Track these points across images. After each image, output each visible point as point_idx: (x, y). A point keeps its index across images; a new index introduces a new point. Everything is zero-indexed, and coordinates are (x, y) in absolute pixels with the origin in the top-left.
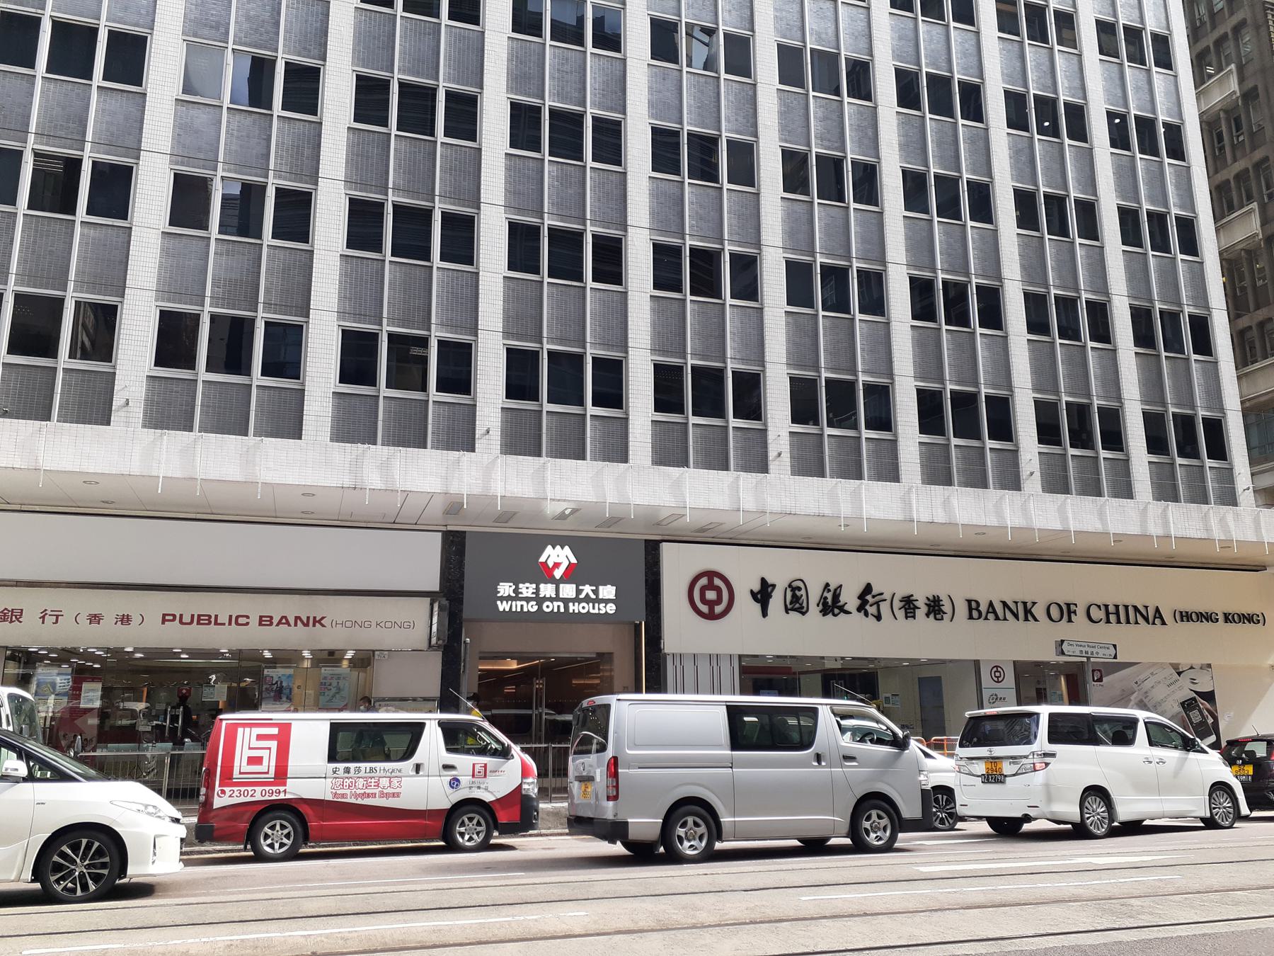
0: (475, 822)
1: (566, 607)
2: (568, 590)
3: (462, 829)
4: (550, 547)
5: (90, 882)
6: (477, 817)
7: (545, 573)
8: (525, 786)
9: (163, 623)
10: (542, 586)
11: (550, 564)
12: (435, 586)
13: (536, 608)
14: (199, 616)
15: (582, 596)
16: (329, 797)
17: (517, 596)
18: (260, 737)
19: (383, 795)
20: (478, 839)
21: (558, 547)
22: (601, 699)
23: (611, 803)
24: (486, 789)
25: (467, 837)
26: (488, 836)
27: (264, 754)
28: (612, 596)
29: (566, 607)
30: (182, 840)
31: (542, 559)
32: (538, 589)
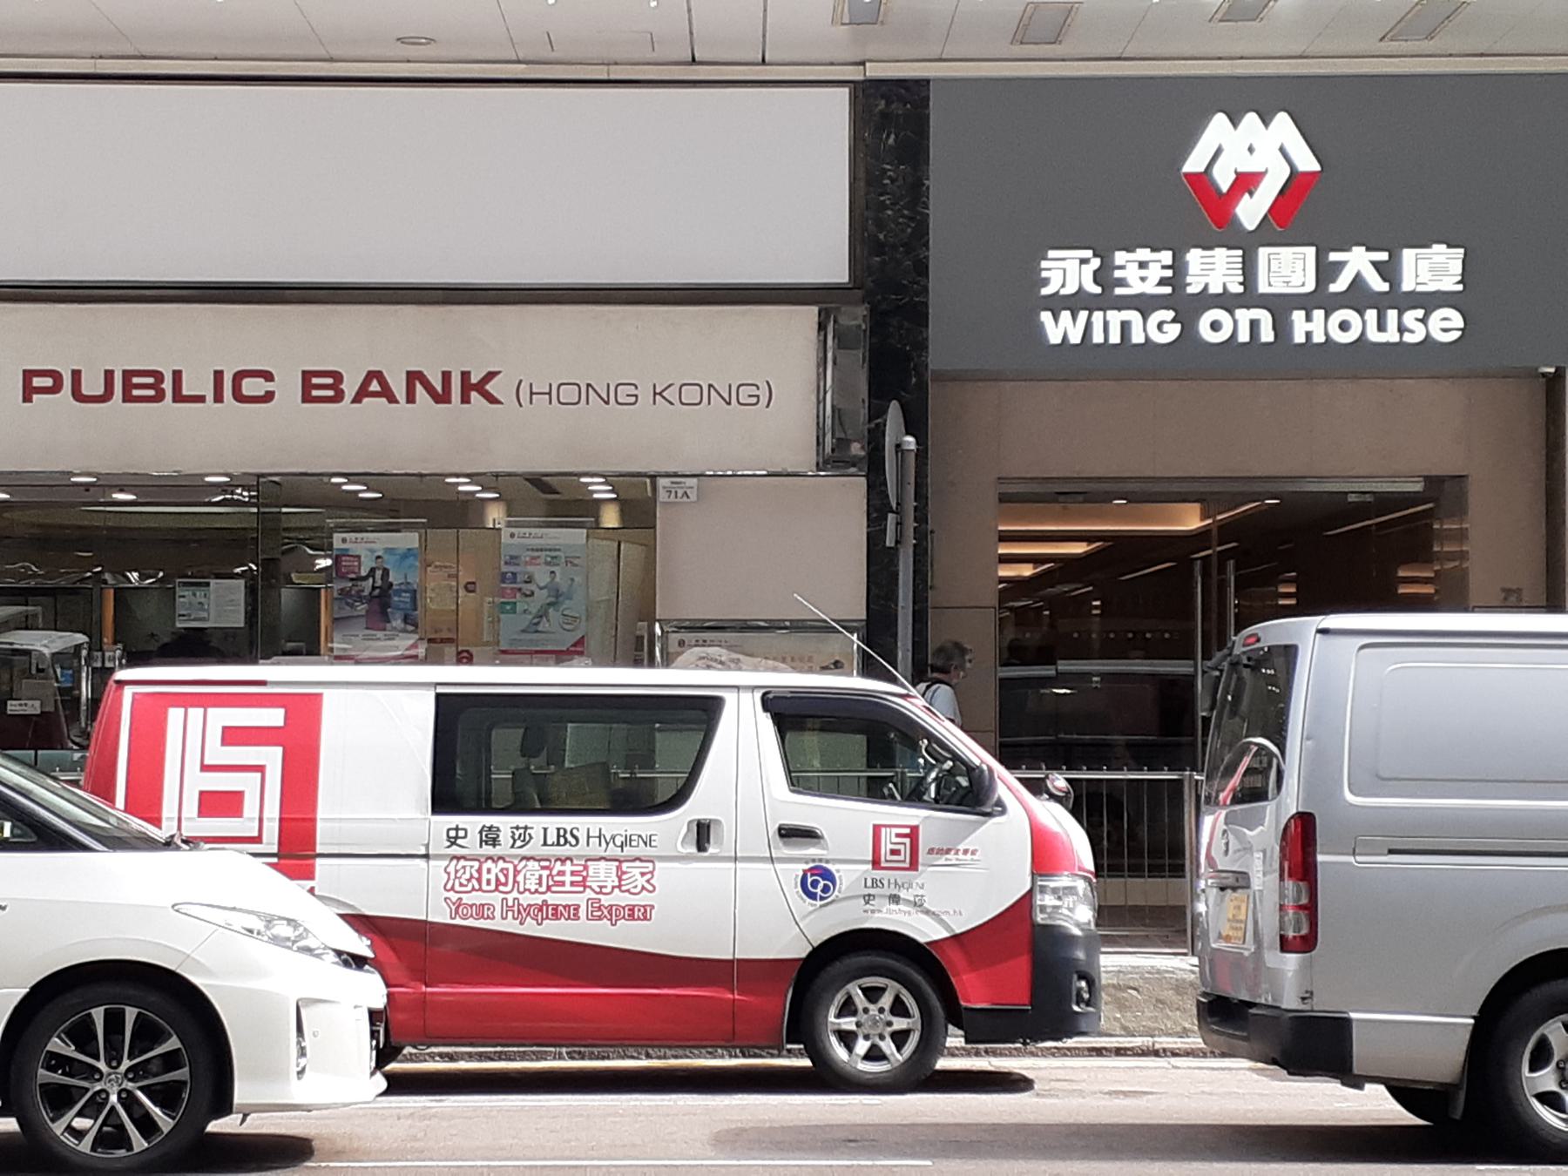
0: (886, 1001)
1: (1282, 327)
2: (1287, 269)
3: (848, 1023)
4: (1220, 120)
5: (156, 1111)
6: (893, 988)
7: (1208, 212)
8: (1039, 900)
9: (27, 398)
10: (1194, 257)
11: (1224, 179)
12: (836, 270)
13: (1173, 331)
14: (128, 375)
15: (1340, 285)
16: (441, 916)
17: (1107, 294)
18: (232, 736)
19: (600, 912)
20: (897, 1057)
21: (1251, 119)
22: (1274, 631)
23: (1292, 960)
24: (917, 904)
25: (862, 1046)
26: (930, 1044)
27: (246, 783)
28: (1451, 284)
29: (1282, 327)
30: (374, 1015)
31: (1194, 163)
32: (1178, 268)
